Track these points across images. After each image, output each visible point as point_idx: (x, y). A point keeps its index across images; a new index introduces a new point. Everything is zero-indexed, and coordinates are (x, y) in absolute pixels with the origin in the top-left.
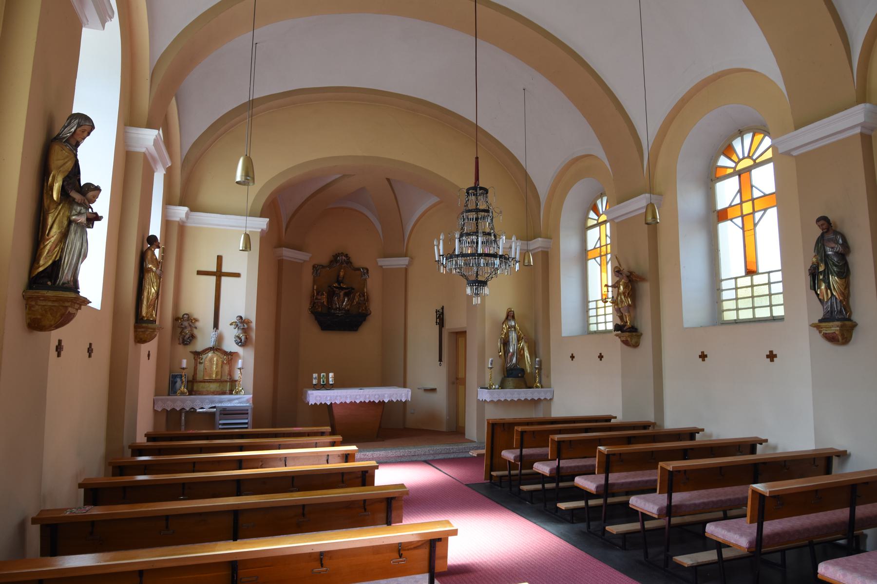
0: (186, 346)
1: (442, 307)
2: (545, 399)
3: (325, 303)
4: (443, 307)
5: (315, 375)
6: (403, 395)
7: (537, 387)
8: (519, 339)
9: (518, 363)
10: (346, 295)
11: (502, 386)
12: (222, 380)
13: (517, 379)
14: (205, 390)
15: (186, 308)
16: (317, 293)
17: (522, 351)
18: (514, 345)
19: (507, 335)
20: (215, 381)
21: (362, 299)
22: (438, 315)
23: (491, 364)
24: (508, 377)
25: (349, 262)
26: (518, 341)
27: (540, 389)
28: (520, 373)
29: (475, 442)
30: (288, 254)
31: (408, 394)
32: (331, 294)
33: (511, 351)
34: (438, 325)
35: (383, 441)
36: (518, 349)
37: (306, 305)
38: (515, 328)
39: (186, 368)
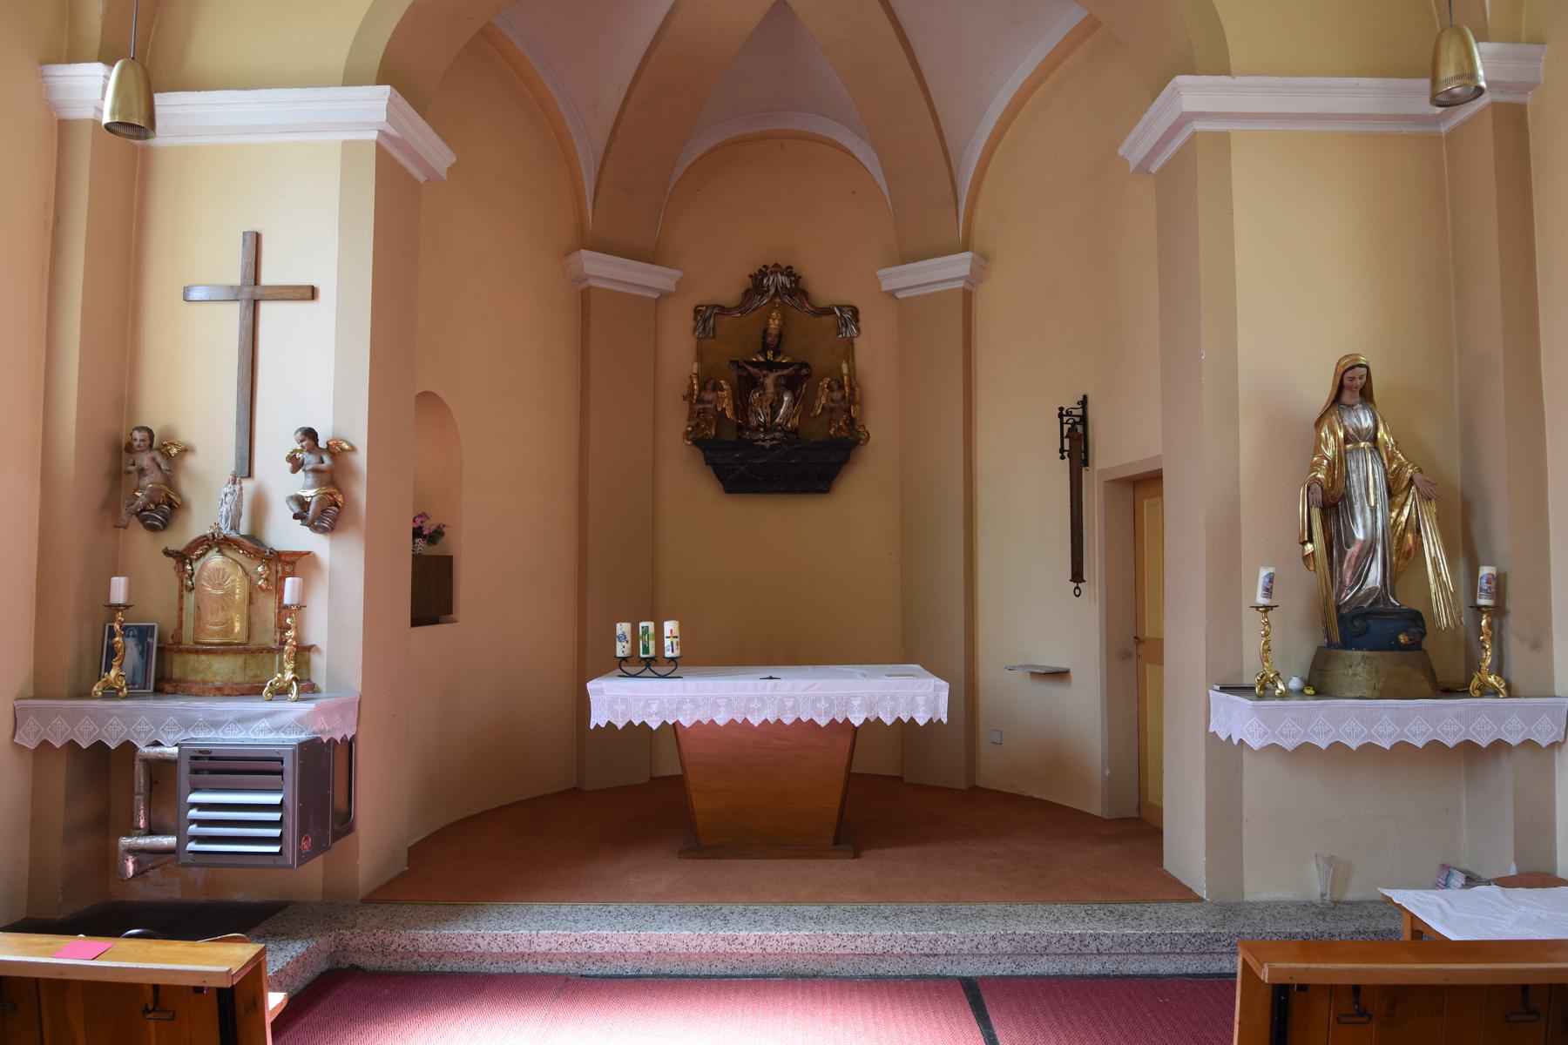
0: (160, 534)
1: (1081, 398)
2: (1529, 744)
3: (729, 414)
4: (1085, 397)
5: (623, 628)
6: (920, 700)
7: (1487, 691)
8: (1394, 490)
9: (1393, 581)
10: (792, 384)
11: (1319, 684)
12: (254, 644)
13: (1397, 653)
14: (198, 678)
15: (156, 413)
16: (699, 384)
17: (1410, 536)
18: (1374, 510)
19: (1339, 468)
20: (226, 649)
21: (837, 395)
22: (1066, 427)
23: (1268, 591)
24: (1346, 645)
25: (796, 289)
26: (1391, 493)
27: (1502, 701)
28: (1405, 631)
29: (1200, 900)
30: (600, 268)
31: (936, 699)
32: (746, 384)
33: (1360, 535)
34: (1067, 459)
35: (856, 855)
36: (1391, 527)
37: (676, 420)
38: (1374, 439)
39: (127, 607)
